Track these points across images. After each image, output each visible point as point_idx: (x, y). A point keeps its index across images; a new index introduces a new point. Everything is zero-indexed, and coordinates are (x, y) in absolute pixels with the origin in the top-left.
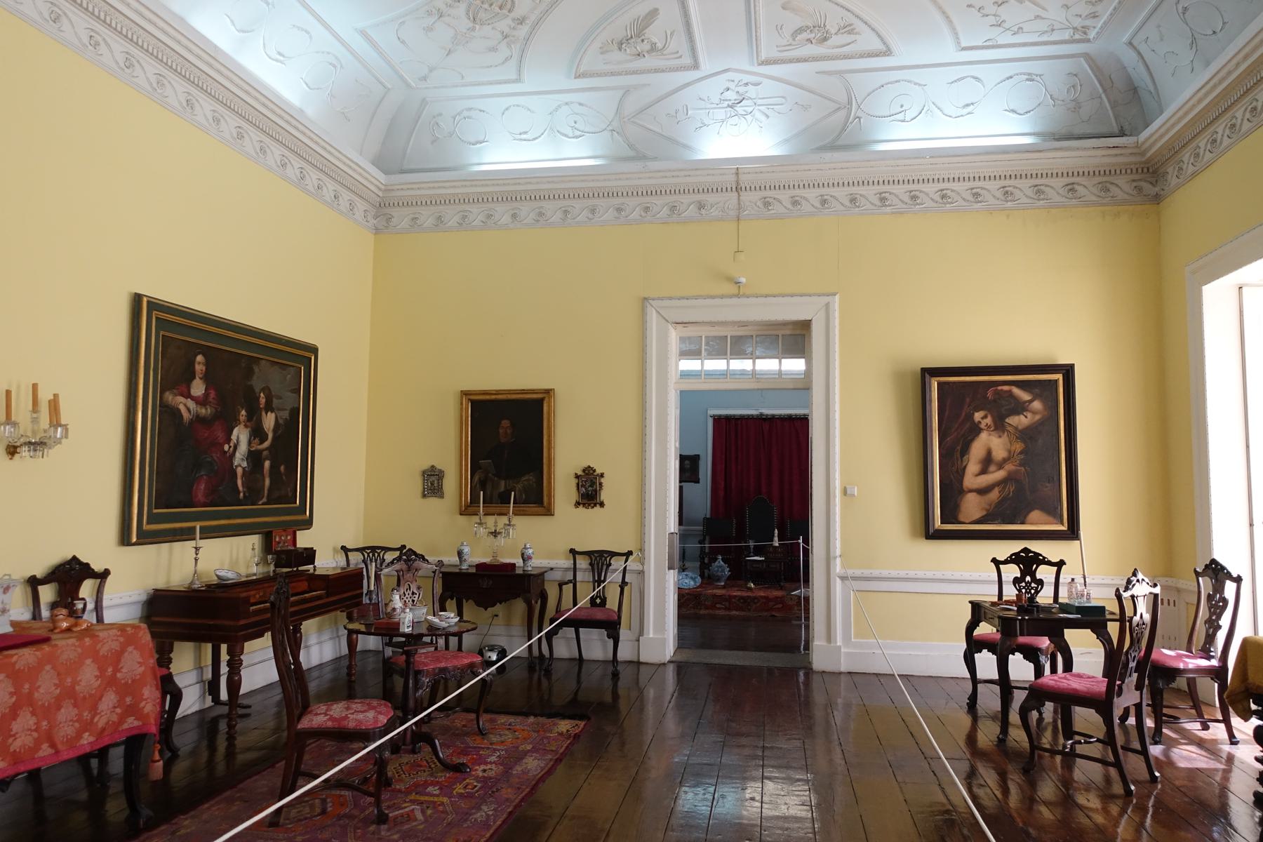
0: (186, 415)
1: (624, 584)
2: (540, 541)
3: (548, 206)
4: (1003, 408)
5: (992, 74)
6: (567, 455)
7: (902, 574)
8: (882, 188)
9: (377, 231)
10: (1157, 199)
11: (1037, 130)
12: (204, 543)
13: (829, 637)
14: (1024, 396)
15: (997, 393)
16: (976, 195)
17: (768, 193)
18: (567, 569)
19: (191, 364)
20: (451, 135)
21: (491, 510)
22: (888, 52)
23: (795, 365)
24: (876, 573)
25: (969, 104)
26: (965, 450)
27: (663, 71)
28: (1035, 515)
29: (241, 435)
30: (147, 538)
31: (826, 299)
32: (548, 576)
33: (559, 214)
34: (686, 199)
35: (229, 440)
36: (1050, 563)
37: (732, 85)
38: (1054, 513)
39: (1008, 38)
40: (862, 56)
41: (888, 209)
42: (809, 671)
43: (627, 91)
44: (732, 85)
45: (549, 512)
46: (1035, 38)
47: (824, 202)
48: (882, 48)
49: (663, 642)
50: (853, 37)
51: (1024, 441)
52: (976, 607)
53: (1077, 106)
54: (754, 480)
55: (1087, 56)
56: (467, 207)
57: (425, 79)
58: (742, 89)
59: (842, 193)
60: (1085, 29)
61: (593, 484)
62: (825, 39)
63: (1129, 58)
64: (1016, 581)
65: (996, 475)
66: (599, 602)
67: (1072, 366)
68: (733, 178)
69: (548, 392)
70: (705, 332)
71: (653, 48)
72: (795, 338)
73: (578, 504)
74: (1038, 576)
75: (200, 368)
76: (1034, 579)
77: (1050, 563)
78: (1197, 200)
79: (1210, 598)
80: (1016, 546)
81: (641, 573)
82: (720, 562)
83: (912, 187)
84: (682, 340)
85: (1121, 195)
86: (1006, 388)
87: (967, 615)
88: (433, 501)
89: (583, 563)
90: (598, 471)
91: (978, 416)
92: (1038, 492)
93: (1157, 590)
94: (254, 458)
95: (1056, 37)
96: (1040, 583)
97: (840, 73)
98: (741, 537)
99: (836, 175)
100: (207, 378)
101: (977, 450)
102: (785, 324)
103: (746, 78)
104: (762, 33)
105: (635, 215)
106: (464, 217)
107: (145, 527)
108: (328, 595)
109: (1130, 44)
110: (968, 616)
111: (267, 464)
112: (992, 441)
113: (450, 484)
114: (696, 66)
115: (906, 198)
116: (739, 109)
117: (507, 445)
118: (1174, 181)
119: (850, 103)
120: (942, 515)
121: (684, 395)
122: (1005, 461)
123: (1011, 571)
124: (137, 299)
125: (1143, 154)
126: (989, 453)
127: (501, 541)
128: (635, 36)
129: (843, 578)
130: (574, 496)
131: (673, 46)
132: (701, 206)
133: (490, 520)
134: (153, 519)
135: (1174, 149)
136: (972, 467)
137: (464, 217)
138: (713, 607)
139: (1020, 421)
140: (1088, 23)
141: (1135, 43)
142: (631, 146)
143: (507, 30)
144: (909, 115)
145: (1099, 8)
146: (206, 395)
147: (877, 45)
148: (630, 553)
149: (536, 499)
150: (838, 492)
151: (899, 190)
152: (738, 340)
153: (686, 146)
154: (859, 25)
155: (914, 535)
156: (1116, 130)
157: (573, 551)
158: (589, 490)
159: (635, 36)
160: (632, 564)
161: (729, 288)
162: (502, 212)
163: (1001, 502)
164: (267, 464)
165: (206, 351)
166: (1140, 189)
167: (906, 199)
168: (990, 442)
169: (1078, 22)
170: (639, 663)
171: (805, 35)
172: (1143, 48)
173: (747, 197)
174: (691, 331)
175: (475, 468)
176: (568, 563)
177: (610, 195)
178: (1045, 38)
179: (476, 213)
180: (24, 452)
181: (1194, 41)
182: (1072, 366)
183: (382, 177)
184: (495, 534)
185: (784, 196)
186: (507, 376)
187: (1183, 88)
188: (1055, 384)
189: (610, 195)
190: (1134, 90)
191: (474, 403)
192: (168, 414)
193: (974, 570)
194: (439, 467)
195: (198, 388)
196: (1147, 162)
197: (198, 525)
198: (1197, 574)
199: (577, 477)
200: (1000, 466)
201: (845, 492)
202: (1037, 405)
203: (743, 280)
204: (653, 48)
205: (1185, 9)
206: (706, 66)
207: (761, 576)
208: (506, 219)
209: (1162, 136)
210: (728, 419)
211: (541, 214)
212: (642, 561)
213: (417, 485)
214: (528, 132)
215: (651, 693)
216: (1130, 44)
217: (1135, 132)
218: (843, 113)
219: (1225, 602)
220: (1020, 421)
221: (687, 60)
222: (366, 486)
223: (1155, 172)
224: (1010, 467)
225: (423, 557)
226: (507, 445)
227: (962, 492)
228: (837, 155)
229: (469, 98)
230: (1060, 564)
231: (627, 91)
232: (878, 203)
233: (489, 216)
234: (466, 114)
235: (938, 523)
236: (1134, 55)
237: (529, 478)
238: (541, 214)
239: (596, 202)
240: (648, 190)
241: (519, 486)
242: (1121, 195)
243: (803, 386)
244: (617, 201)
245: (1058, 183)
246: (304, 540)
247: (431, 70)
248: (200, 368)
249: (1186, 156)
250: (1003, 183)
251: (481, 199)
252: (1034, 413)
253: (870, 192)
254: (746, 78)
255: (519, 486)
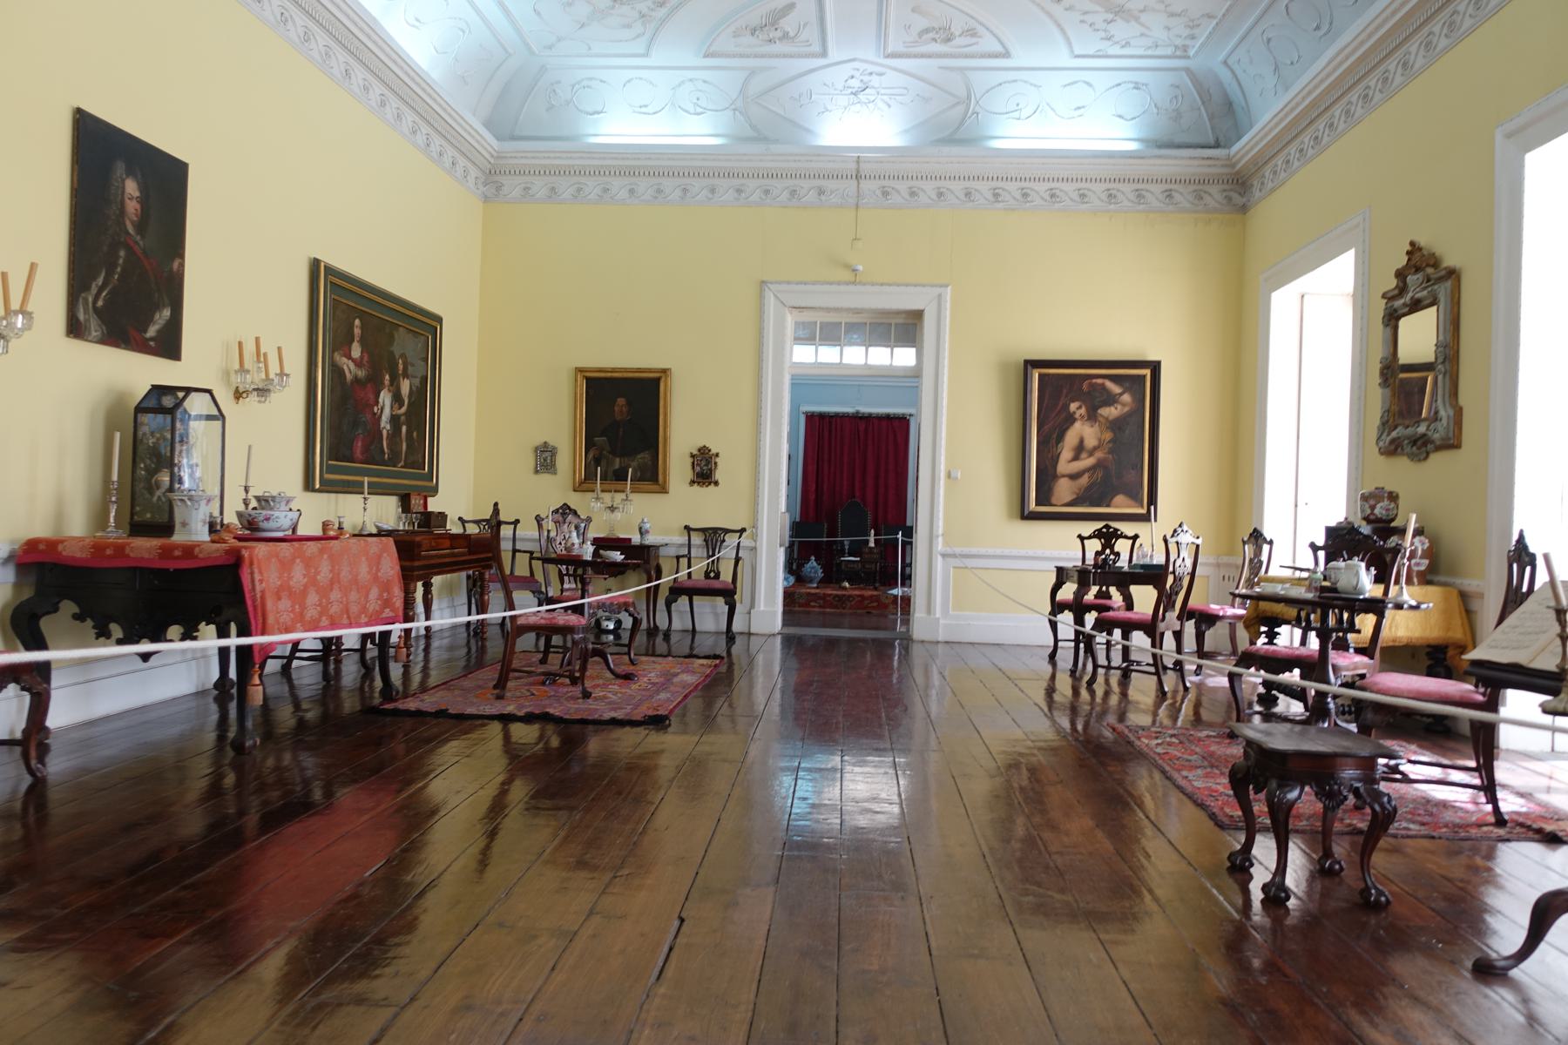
0: (349, 377)
1: (737, 560)
2: (659, 516)
3: (668, 184)
4: (1096, 400)
5: (1102, 81)
6: (682, 433)
7: (998, 552)
8: (995, 184)
9: (486, 199)
10: (1244, 209)
11: (1142, 135)
12: (373, 499)
13: (929, 610)
14: (1115, 389)
15: (1092, 386)
16: (1083, 196)
17: (886, 183)
18: (681, 545)
19: (351, 326)
20: (568, 103)
21: (606, 487)
22: (1006, 54)
23: (905, 357)
24: (974, 551)
25: (1079, 106)
26: (1061, 438)
27: (791, 57)
28: (1120, 499)
29: (385, 398)
30: (329, 487)
31: (938, 290)
32: (662, 551)
33: (678, 192)
34: (806, 184)
35: (377, 403)
36: (1126, 537)
37: (857, 74)
38: (1135, 497)
39: (1116, 50)
40: (983, 56)
41: (1001, 205)
42: (907, 640)
43: (753, 72)
44: (857, 74)
45: (664, 490)
46: (1141, 52)
47: (940, 195)
48: (999, 49)
49: (775, 613)
50: (974, 40)
51: (1113, 430)
52: (1060, 570)
53: (1177, 116)
54: (856, 475)
55: (1188, 70)
56: (583, 179)
57: (550, 47)
58: (866, 78)
59: (958, 187)
60: (1185, 48)
61: (708, 462)
62: (949, 40)
63: (1225, 75)
64: (1098, 554)
65: (1086, 462)
66: (712, 573)
67: (1159, 363)
68: (854, 166)
69: (665, 371)
70: (820, 318)
71: (785, 36)
72: (905, 327)
73: (692, 482)
74: (1116, 549)
75: (357, 331)
76: (1112, 552)
77: (1126, 537)
78: (1277, 210)
79: (1251, 561)
80: (1099, 525)
81: (754, 549)
82: (813, 563)
83: (1023, 184)
84: (797, 324)
85: (1212, 203)
86: (1099, 381)
87: (1053, 579)
88: (545, 478)
89: (697, 539)
90: (714, 451)
91: (1073, 406)
92: (1126, 474)
93: (1199, 542)
94: (394, 419)
95: (1159, 52)
96: (1118, 554)
97: (961, 69)
98: (832, 533)
99: (950, 170)
100: (363, 342)
101: (1071, 438)
102: (898, 313)
103: (871, 68)
104: (891, 31)
105: (755, 197)
106: (579, 190)
107: (327, 476)
108: (470, 553)
109: (1225, 63)
110: (1054, 580)
111: (404, 429)
112: (1083, 429)
113: (564, 461)
114: (824, 54)
115: (1018, 195)
116: (861, 96)
117: (622, 422)
118: (1257, 194)
119: (969, 97)
120: (1036, 501)
121: (793, 377)
122: (1095, 449)
123: (1094, 545)
124: (315, 264)
125: (1233, 166)
126: (1082, 441)
127: (618, 515)
128: (770, 26)
129: (944, 556)
130: (689, 475)
131: (804, 36)
132: (821, 192)
133: (607, 497)
134: (331, 470)
135: (1261, 162)
136: (1066, 454)
137: (579, 190)
138: (807, 605)
139: (1111, 412)
140: (1188, 42)
141: (1230, 62)
142: (753, 127)
143: (645, 11)
144: (1025, 113)
145: (1196, 31)
146: (362, 357)
147: (999, 48)
148: (743, 530)
149: (651, 477)
150: (943, 475)
151: (1013, 187)
152: (852, 327)
153: (808, 131)
154: (980, 29)
155: (1011, 516)
156: (1212, 141)
157: (686, 527)
158: (704, 470)
159: (770, 26)
160: (746, 541)
161: (847, 275)
162: (618, 186)
163: (1089, 488)
164: (404, 429)
165: (363, 315)
166: (1229, 199)
167: (1018, 196)
168: (1083, 431)
169: (1179, 42)
170: (750, 634)
171: (931, 35)
172: (1235, 67)
173: (866, 185)
174: (807, 317)
175: (589, 445)
176: (684, 539)
177: (730, 175)
178: (1149, 52)
179: (592, 186)
180: (254, 397)
181: (1276, 68)
182: (1159, 363)
183: (494, 143)
184: (612, 509)
185: (903, 186)
186: (623, 354)
187: (1268, 109)
188: (1142, 378)
189: (730, 175)
190: (1229, 105)
191: (588, 380)
192: (336, 372)
193: (1066, 544)
194: (551, 443)
195: (356, 351)
196: (1238, 173)
197: (366, 479)
198: (1244, 543)
199: (693, 456)
200: (1091, 454)
201: (949, 475)
202: (1126, 398)
203: (860, 268)
204: (785, 36)
205: (1269, 40)
206: (834, 54)
207: (854, 578)
208: (624, 194)
209: (1257, 144)
210: (822, 417)
211: (659, 191)
212: (754, 537)
213: (530, 461)
214: (651, 106)
215: (760, 659)
216: (1225, 63)
217: (1228, 146)
218: (960, 109)
219: (1261, 563)
220: (1111, 412)
221: (816, 48)
222: (491, 455)
223: (1244, 183)
224: (1099, 454)
225: (575, 513)
226: (622, 422)
227: (1055, 477)
228: (955, 150)
229: (586, 68)
230: (1135, 537)
231: (753, 72)
232: (991, 198)
233: (606, 190)
234: (585, 83)
235: (1032, 505)
236: (1229, 73)
237: (644, 457)
238: (659, 191)
239: (716, 181)
240: (767, 173)
241: (634, 464)
242: (1212, 203)
243: (915, 374)
244: (736, 182)
245: (1157, 189)
246: (434, 505)
247: (559, 40)
248: (357, 331)
249: (1267, 171)
250: (1108, 186)
251: (597, 172)
252: (1124, 405)
253: (984, 187)
254: (871, 68)
255: (634, 464)
